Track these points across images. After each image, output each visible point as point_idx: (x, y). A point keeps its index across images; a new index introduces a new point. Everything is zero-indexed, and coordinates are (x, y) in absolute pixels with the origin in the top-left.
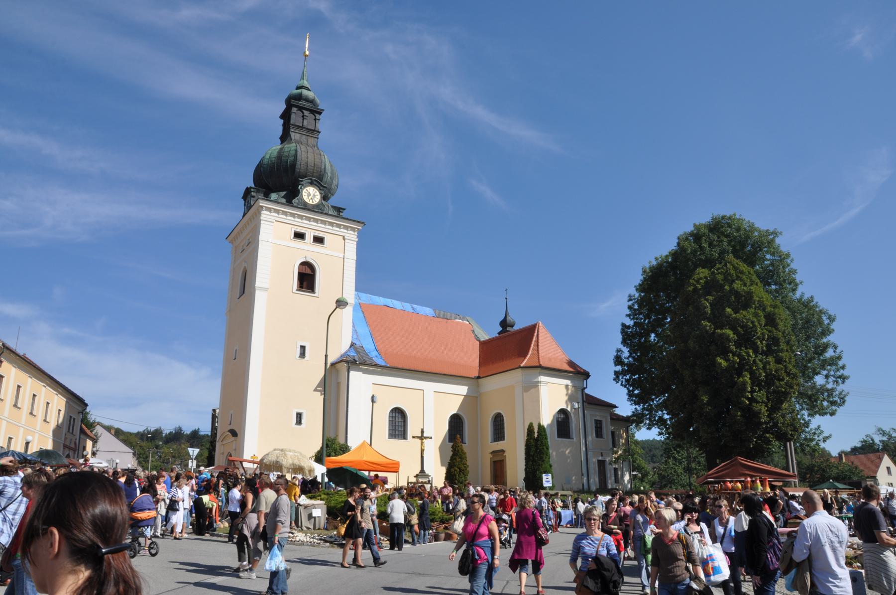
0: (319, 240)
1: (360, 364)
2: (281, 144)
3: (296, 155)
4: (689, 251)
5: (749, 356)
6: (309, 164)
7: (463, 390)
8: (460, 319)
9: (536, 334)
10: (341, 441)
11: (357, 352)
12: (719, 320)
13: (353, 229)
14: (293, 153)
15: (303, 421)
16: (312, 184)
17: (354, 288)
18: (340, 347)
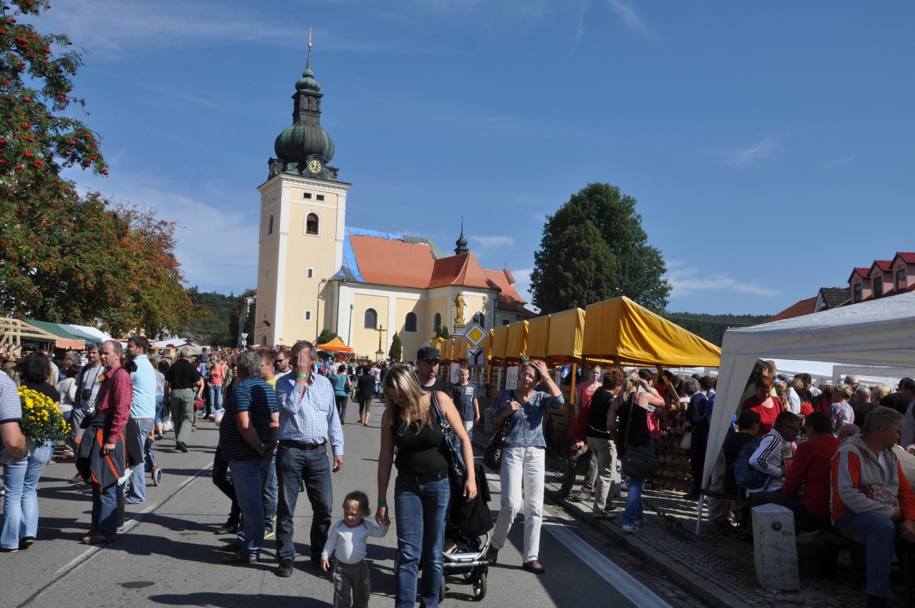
0: (320, 198)
1: (347, 282)
2: (293, 124)
3: (304, 137)
4: (570, 211)
5: (579, 290)
6: (314, 140)
7: (417, 296)
8: (423, 242)
9: (465, 263)
10: (334, 331)
11: (345, 273)
12: (568, 266)
13: (344, 189)
14: (302, 134)
15: (311, 317)
16: (315, 158)
17: (344, 225)
18: (334, 268)
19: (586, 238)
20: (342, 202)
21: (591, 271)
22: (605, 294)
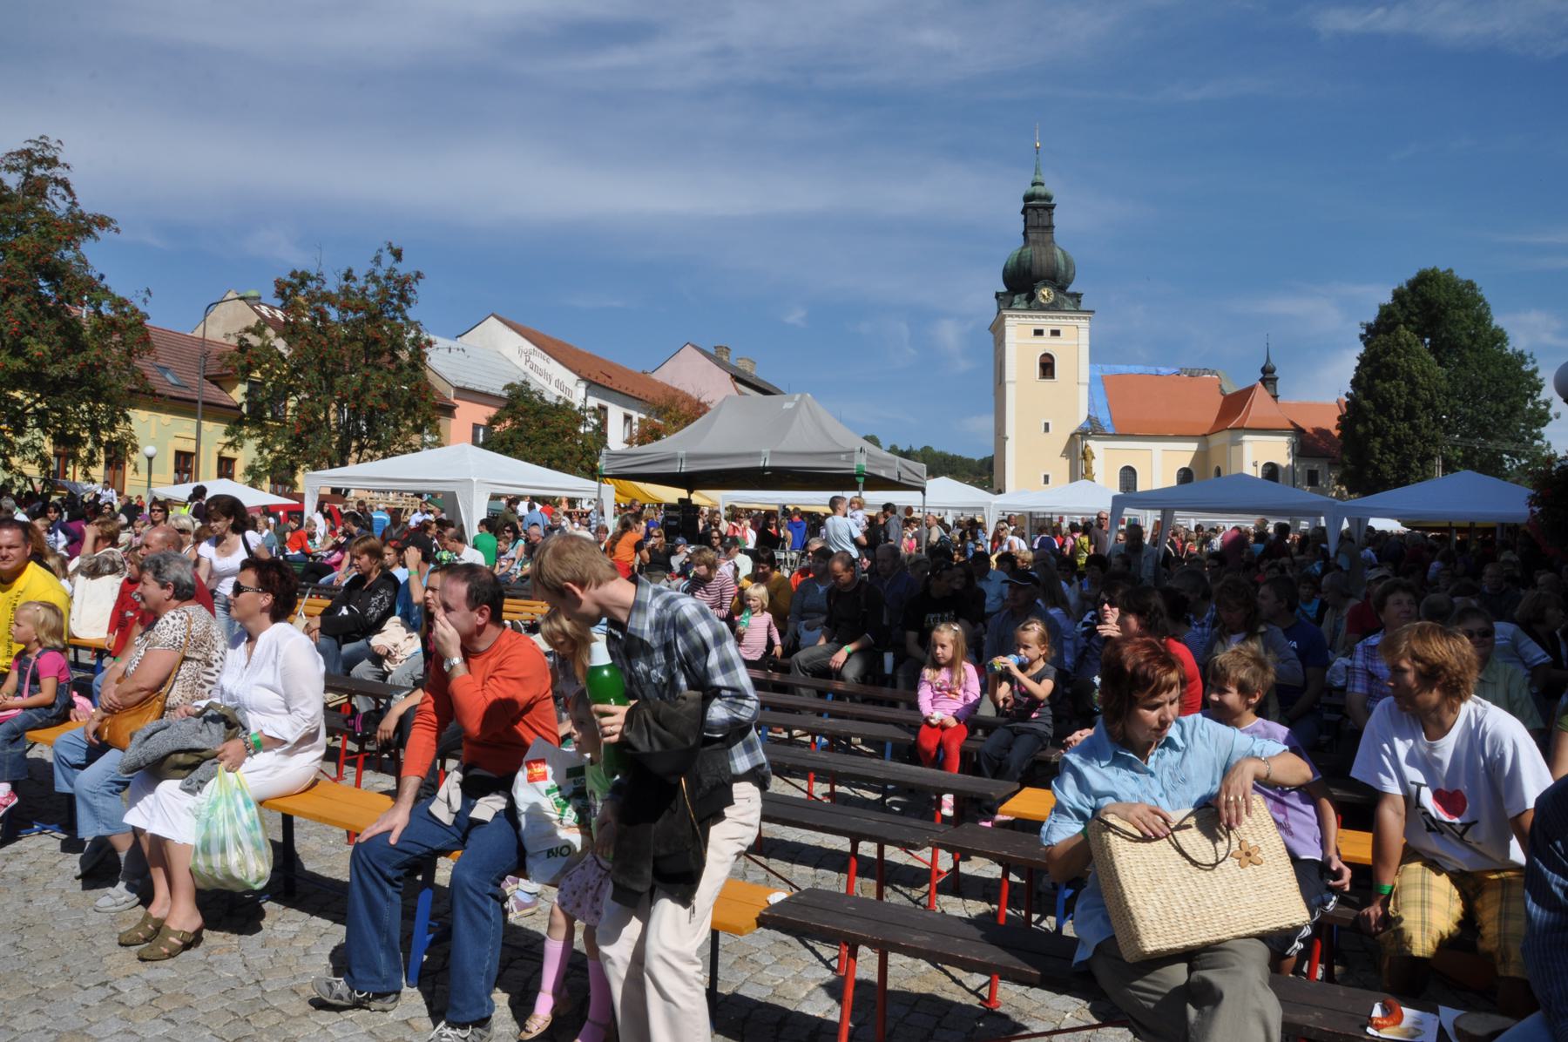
0: (1055, 333)
3: (1031, 261)
5: (1383, 423)
13: (1085, 318)
16: (1046, 285)
19: (1395, 350)
20: (1084, 336)
21: (1400, 396)
22: (1423, 426)
